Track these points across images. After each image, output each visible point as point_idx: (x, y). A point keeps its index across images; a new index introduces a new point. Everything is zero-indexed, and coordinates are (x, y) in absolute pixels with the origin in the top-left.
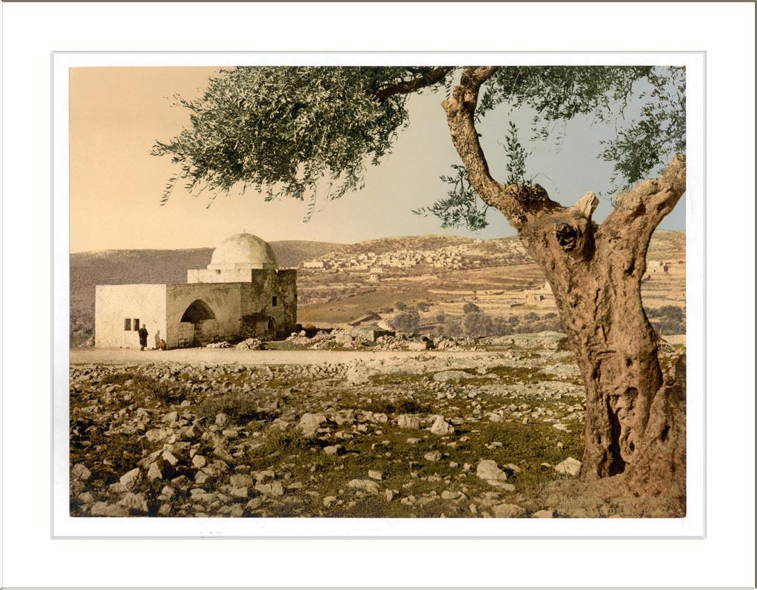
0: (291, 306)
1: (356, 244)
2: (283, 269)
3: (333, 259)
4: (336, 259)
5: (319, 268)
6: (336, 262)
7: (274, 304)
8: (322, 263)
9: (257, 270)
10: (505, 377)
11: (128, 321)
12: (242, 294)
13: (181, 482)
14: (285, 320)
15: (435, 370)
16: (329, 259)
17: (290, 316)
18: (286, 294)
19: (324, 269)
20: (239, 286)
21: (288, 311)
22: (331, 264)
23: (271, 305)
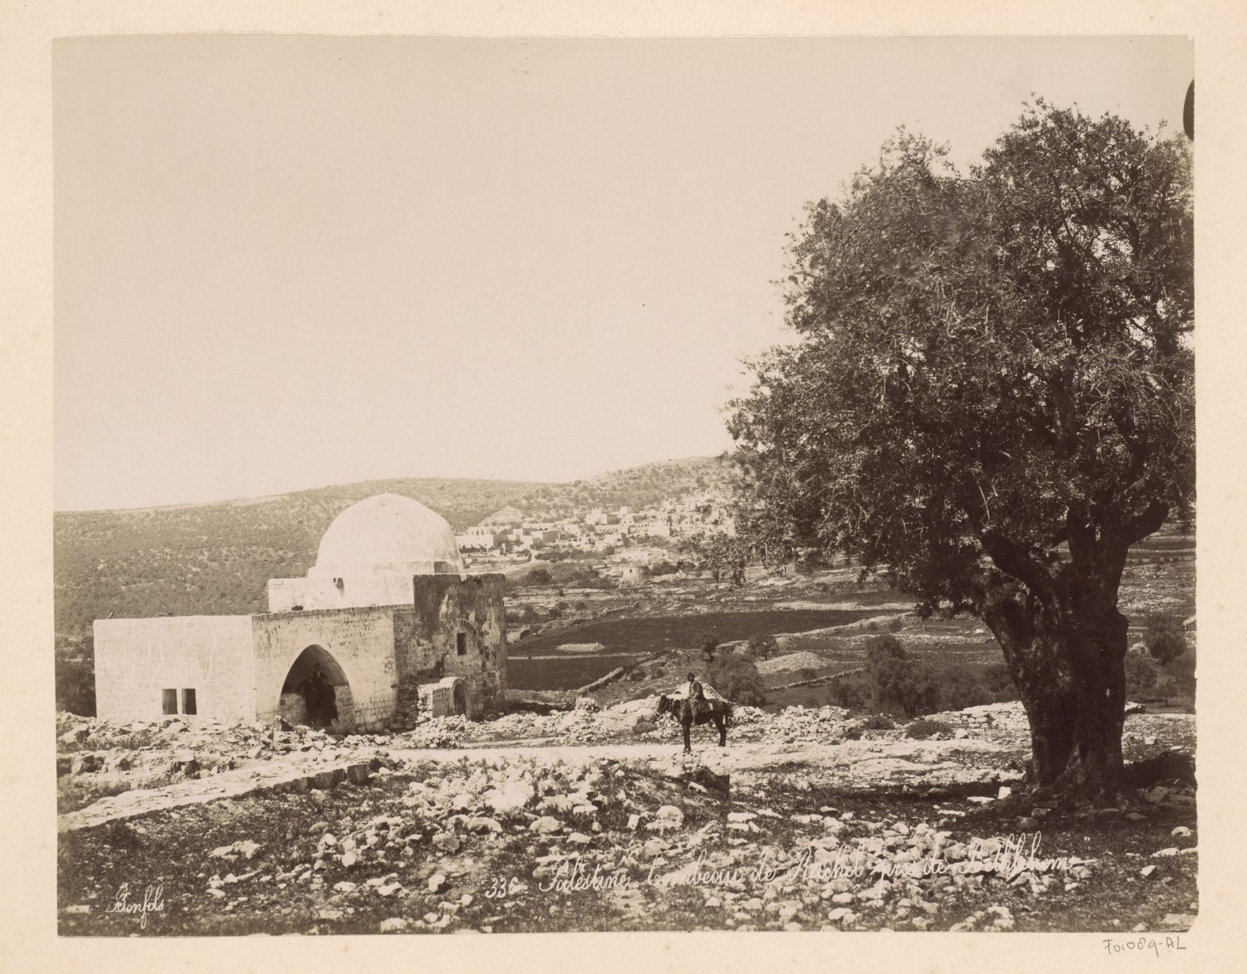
0: (494, 655)
1: (577, 484)
2: (1127, 675)
3: (518, 526)
4: (526, 525)
5: (483, 549)
6: (527, 533)
7: (462, 651)
8: (492, 537)
9: (425, 577)
10: (1001, 820)
11: (171, 693)
12: (397, 630)
13: (1024, 592)
14: (485, 684)
15: (853, 759)
16: (508, 527)
17: (494, 675)
18: (485, 627)
19: (497, 553)
20: (391, 613)
21: (489, 664)
22: (512, 537)
23: (456, 652)
